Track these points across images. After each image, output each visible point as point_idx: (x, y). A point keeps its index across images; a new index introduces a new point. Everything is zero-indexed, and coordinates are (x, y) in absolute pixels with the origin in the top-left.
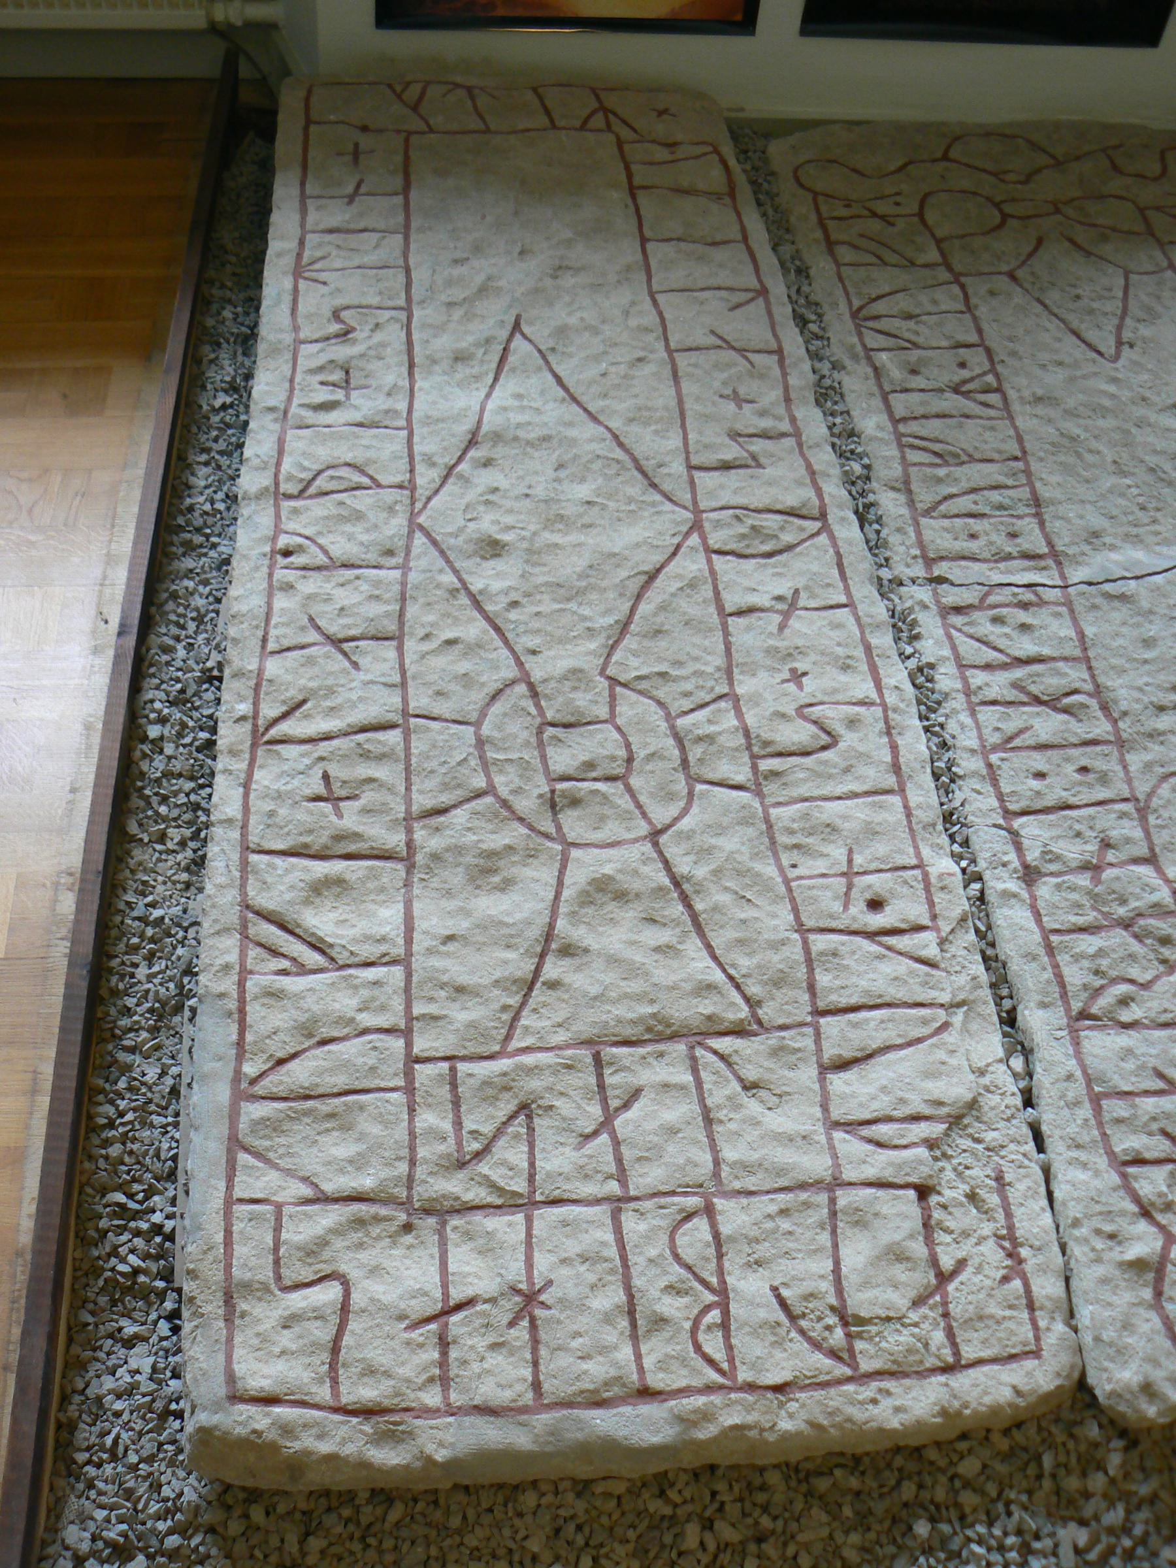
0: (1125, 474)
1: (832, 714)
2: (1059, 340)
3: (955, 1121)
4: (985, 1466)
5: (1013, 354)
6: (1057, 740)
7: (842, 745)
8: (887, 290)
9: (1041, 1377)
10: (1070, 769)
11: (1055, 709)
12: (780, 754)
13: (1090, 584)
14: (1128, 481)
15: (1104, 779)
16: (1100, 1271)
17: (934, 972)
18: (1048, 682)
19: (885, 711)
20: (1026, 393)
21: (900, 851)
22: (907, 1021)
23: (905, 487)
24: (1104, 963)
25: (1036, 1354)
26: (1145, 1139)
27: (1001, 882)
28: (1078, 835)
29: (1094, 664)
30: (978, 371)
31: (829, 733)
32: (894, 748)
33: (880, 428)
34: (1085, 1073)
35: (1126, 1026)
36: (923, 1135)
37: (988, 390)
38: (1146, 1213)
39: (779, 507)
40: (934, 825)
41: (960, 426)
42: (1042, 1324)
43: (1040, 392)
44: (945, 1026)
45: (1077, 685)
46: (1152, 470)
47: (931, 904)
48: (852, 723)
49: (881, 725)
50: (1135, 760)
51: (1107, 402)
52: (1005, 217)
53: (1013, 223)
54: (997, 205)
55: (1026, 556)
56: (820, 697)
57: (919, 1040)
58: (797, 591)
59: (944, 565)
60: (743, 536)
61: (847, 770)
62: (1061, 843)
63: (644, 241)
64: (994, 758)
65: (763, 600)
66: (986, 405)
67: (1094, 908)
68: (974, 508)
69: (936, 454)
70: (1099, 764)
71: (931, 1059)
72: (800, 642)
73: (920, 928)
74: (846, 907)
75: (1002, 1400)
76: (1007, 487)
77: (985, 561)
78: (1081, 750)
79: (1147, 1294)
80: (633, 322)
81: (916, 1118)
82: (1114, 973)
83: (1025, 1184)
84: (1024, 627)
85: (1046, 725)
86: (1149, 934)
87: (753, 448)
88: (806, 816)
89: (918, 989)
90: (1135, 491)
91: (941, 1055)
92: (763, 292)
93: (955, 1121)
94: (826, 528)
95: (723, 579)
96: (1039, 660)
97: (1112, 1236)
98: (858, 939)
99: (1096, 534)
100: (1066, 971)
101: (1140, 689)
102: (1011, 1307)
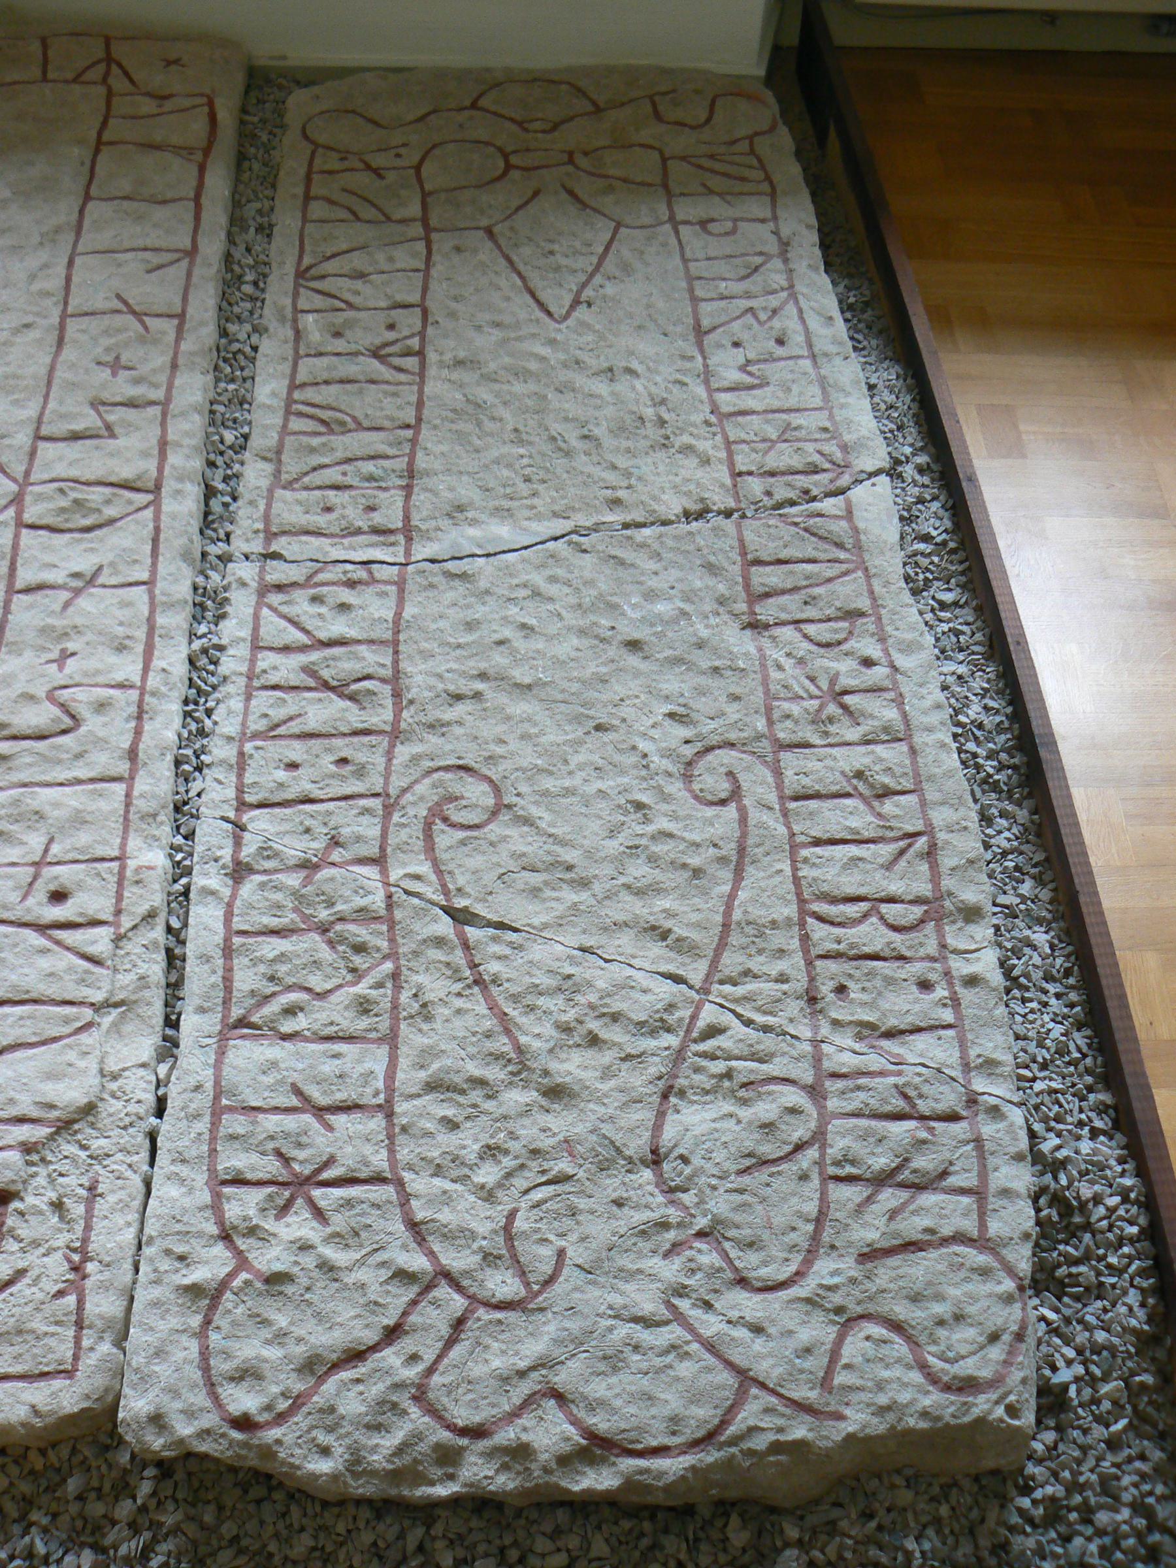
0: (521, 442)
1: (80, 698)
2: (508, 299)
3: (65, 1126)
4: (11, 1484)
5: (453, 315)
6: (323, 730)
7: (83, 730)
8: (344, 247)
9: (65, 1398)
10: (327, 760)
11: (341, 696)
12: (15, 738)
13: (433, 561)
14: (522, 451)
15: (361, 772)
16: (156, 1292)
17: (97, 970)
18: (342, 665)
19: (142, 694)
20: (448, 357)
21: (105, 842)
22: (48, 1020)
23: (275, 456)
24: (283, 969)
25: (69, 1374)
26: (254, 1158)
27: (207, 878)
28: (308, 831)
29: (402, 648)
30: (406, 333)
31: (73, 717)
32: (138, 732)
33: (274, 394)
34: (217, 1083)
35: (285, 1037)
36: (22, 1138)
37: (405, 355)
38: (226, 1236)
39: (113, 479)
40: (154, 816)
41: (360, 391)
42: (86, 1343)
43: (462, 354)
44: (89, 1025)
45: (370, 670)
46: (554, 439)
47: (119, 897)
48: (101, 706)
49: (133, 709)
50: (403, 752)
51: (533, 366)
52: (509, 167)
53: (515, 174)
54: (506, 156)
55: (376, 531)
56: (78, 679)
57: (55, 1040)
58: (100, 568)
59: (283, 540)
60: (63, 510)
61: (79, 756)
62: (287, 840)
63: (87, 197)
64: (248, 747)
65: (56, 577)
66: (400, 370)
67: (296, 910)
68: (340, 479)
69: (323, 422)
70: (361, 757)
71: (59, 1059)
72: (79, 621)
73: (96, 923)
74: (25, 897)
75: (13, 1419)
76: (387, 457)
77: (332, 536)
78: (348, 740)
79: (196, 1321)
80: (36, 286)
81: (21, 1120)
82: (291, 980)
83: (118, 1193)
84: (344, 607)
85: (321, 711)
86: (342, 940)
87: (111, 418)
88: (16, 802)
89: (71, 986)
90: (525, 461)
91: (72, 1056)
92: (192, 253)
93: (65, 1126)
94: (156, 503)
95: (23, 554)
96: (341, 642)
97: (182, 1258)
98: (27, 932)
99: (460, 508)
100: (238, 975)
101: (440, 676)
102: (57, 1323)
